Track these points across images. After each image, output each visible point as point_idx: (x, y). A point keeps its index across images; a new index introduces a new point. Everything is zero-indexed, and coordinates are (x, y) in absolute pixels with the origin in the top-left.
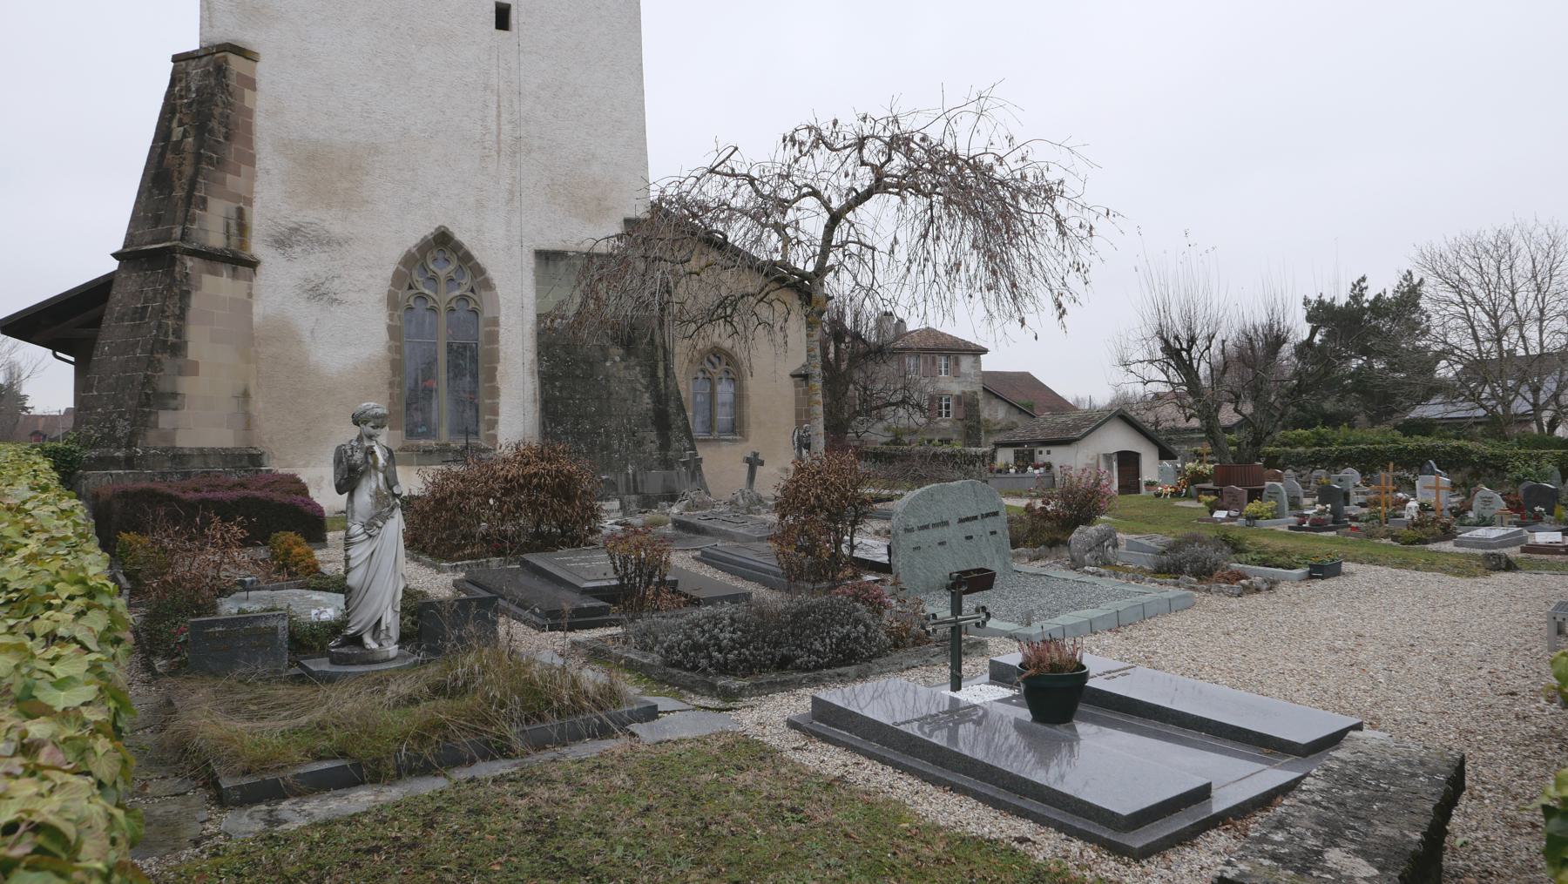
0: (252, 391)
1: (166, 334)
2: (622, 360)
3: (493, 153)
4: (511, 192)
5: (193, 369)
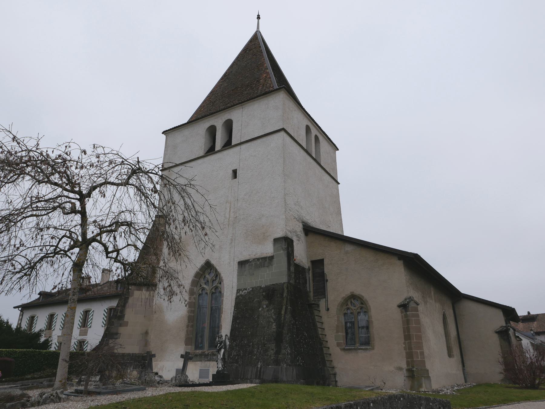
0: (149, 332)
1: (117, 312)
2: (267, 307)
3: (227, 226)
4: (232, 240)
5: (126, 324)
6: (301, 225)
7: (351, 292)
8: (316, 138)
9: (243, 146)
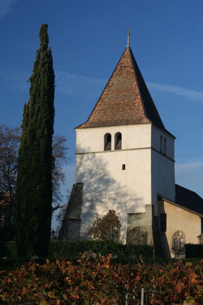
6: (157, 197)
7: (178, 230)
8: (165, 139)
9: (129, 152)
